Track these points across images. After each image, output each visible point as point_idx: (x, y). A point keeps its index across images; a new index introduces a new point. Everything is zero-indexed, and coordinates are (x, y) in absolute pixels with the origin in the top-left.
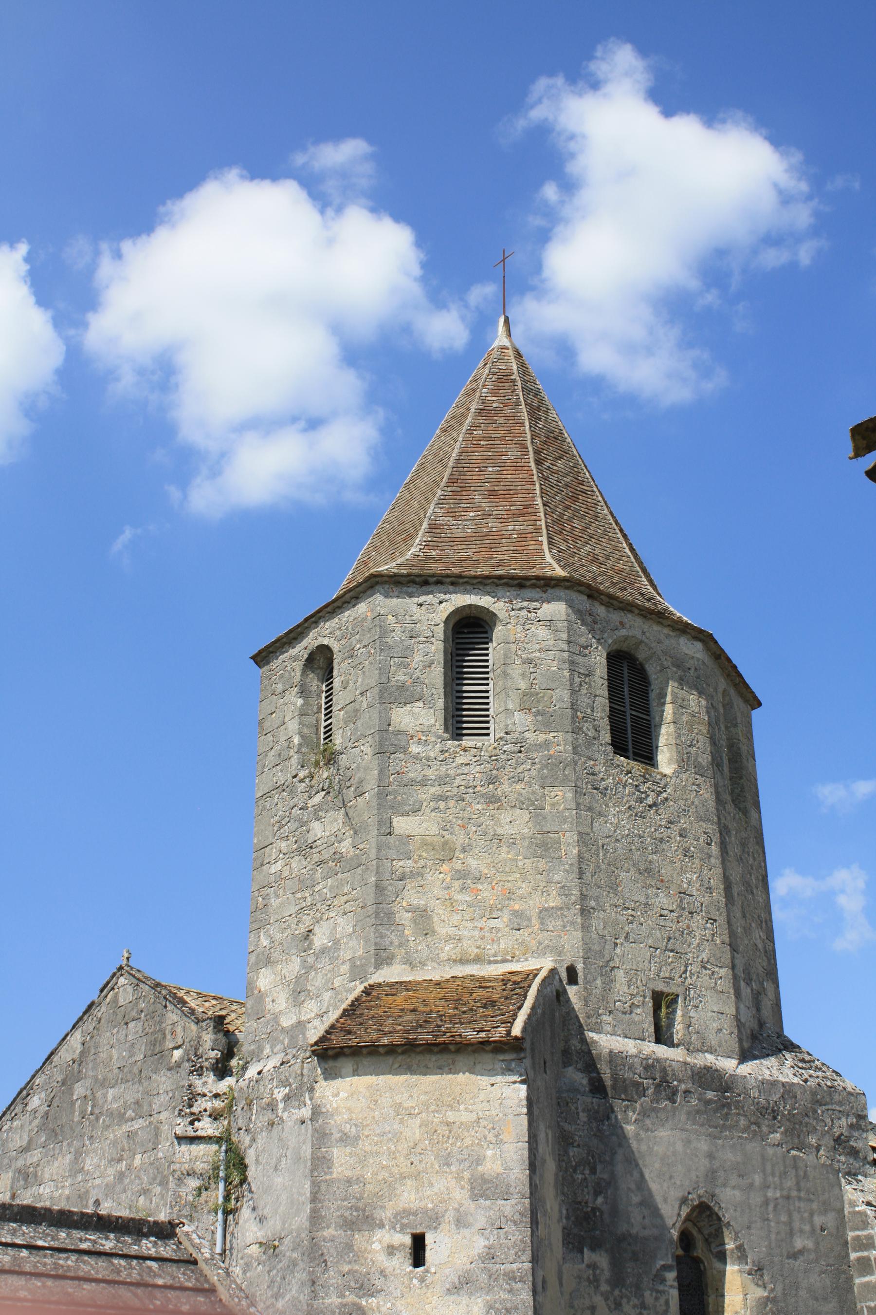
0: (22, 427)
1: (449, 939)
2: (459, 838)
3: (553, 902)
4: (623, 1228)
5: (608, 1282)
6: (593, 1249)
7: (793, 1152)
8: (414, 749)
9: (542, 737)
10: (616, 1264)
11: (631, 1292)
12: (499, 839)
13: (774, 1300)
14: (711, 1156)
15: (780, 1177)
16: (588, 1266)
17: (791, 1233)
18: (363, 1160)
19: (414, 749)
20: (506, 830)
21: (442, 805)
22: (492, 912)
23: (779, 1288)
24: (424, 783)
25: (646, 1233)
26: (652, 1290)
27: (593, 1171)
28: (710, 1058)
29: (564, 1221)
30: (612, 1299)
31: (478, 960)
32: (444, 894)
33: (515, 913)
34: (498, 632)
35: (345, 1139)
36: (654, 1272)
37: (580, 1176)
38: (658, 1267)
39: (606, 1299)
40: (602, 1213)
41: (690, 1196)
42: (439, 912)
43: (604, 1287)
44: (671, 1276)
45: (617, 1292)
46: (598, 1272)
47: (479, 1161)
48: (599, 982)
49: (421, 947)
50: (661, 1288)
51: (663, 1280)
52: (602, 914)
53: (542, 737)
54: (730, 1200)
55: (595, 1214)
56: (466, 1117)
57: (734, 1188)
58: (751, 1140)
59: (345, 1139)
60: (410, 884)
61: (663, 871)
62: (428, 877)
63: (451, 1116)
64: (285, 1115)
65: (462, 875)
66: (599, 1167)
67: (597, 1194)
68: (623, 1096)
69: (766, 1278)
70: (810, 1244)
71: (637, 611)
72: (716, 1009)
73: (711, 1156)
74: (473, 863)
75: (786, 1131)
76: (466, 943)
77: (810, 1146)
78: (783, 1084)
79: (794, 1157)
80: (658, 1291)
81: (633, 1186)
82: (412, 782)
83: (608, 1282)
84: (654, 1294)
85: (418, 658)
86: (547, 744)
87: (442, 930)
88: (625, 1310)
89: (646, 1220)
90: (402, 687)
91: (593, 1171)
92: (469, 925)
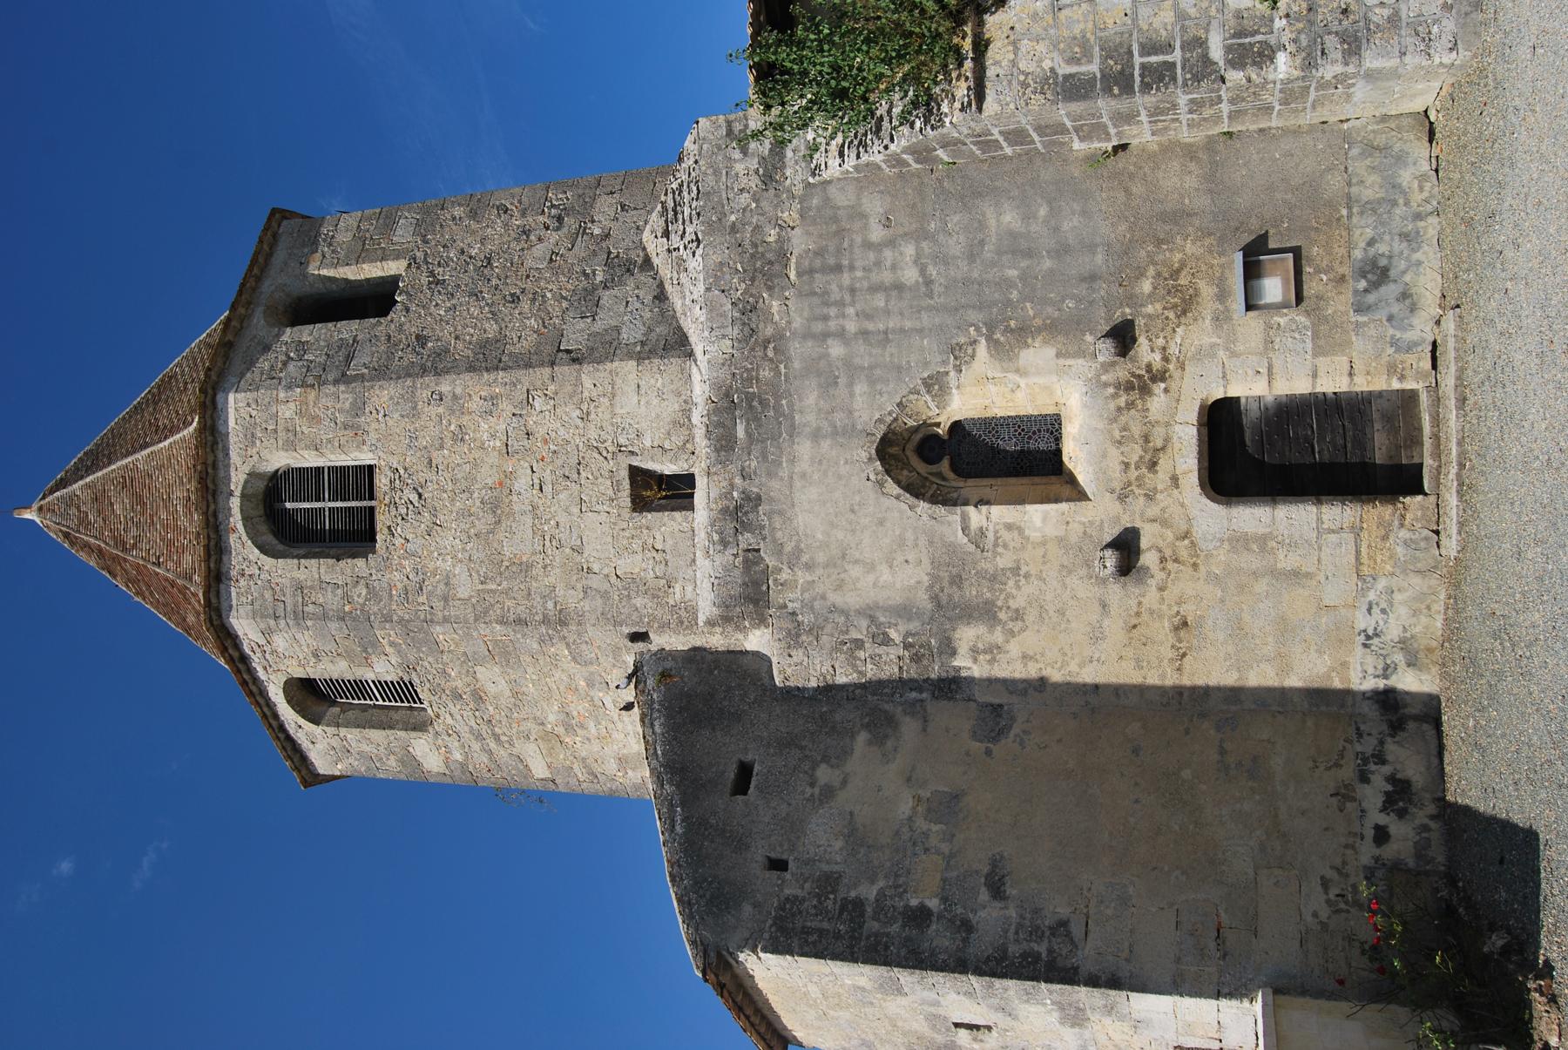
4: (923, 600)
5: (991, 628)
6: (954, 653)
7: (793, 275)
8: (458, 756)
10: (970, 613)
11: (1001, 591)
13: (991, 327)
14: (816, 436)
15: (827, 304)
16: (975, 660)
17: (899, 287)
21: (503, 738)
23: (973, 316)
25: (926, 561)
26: (995, 554)
27: (859, 644)
28: (699, 433)
29: (924, 695)
30: (1011, 625)
34: (299, 673)
36: (972, 548)
37: (870, 666)
38: (965, 540)
39: (1012, 633)
40: (908, 634)
41: (872, 477)
43: (998, 636)
44: (976, 516)
45: (1002, 615)
46: (980, 646)
48: (638, 602)
50: (990, 535)
51: (982, 532)
52: (560, 592)
54: (872, 408)
55: (911, 645)
57: (852, 395)
58: (789, 359)
60: (598, 769)
61: (490, 481)
62: (584, 754)
66: (855, 635)
67: (887, 641)
68: (764, 588)
69: (962, 340)
70: (909, 250)
71: (212, 507)
72: (635, 399)
73: (816, 436)
75: (770, 289)
77: (780, 240)
78: (708, 289)
79: (799, 275)
80: (996, 545)
81: (871, 578)
83: (991, 628)
84: (1000, 550)
86: (392, 644)
88: (1023, 604)
89: (910, 558)
90: (401, 761)
91: (859, 644)
92: (620, 726)
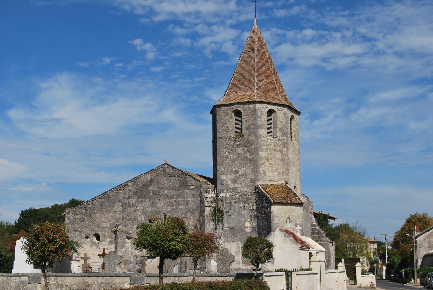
0: (127, 7)
1: (269, 176)
2: (270, 157)
3: (284, 171)
8: (263, 139)
9: (283, 138)
12: (276, 158)
18: (279, 220)
19: (263, 139)
20: (277, 156)
22: (274, 172)
24: (264, 145)
31: (273, 181)
32: (267, 168)
33: (279, 172)
35: (277, 217)
42: (267, 171)
47: (296, 221)
49: (264, 177)
53: (283, 138)
56: (294, 214)
59: (277, 217)
60: (262, 166)
63: (292, 214)
64: (235, 205)
65: (270, 164)
74: (272, 162)
76: (271, 177)
82: (263, 145)
85: (263, 119)
86: (283, 140)
87: (268, 175)
